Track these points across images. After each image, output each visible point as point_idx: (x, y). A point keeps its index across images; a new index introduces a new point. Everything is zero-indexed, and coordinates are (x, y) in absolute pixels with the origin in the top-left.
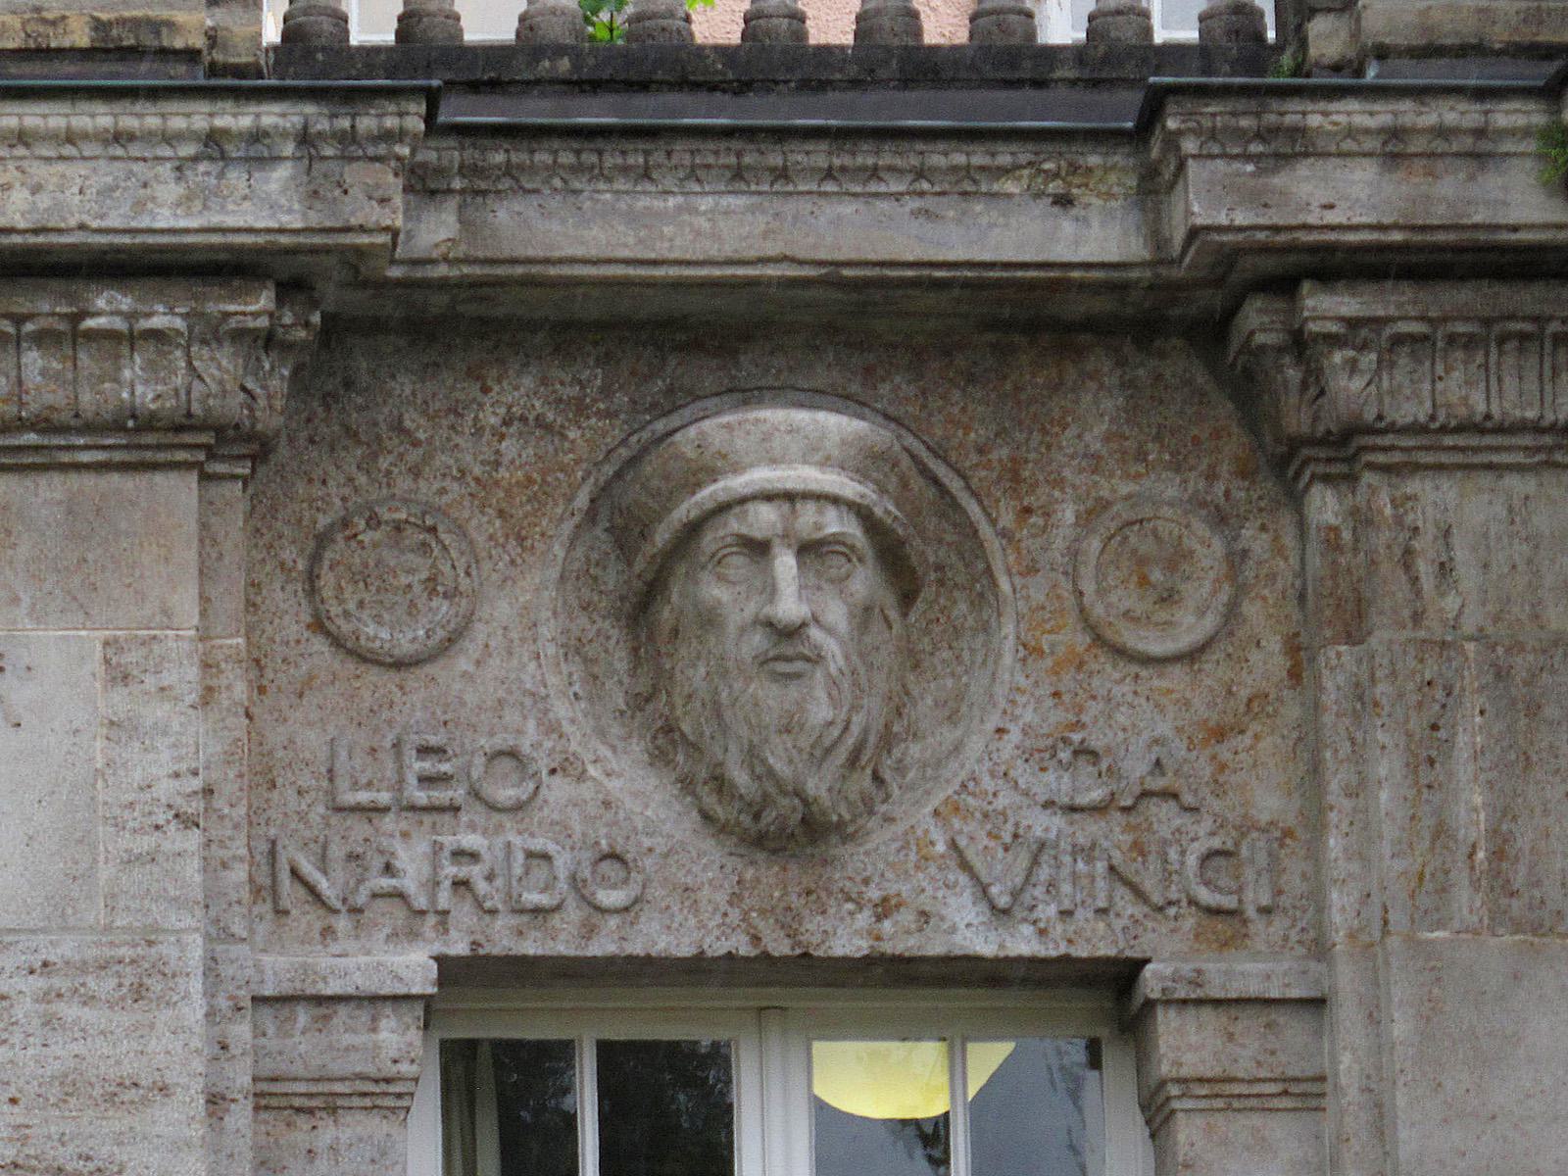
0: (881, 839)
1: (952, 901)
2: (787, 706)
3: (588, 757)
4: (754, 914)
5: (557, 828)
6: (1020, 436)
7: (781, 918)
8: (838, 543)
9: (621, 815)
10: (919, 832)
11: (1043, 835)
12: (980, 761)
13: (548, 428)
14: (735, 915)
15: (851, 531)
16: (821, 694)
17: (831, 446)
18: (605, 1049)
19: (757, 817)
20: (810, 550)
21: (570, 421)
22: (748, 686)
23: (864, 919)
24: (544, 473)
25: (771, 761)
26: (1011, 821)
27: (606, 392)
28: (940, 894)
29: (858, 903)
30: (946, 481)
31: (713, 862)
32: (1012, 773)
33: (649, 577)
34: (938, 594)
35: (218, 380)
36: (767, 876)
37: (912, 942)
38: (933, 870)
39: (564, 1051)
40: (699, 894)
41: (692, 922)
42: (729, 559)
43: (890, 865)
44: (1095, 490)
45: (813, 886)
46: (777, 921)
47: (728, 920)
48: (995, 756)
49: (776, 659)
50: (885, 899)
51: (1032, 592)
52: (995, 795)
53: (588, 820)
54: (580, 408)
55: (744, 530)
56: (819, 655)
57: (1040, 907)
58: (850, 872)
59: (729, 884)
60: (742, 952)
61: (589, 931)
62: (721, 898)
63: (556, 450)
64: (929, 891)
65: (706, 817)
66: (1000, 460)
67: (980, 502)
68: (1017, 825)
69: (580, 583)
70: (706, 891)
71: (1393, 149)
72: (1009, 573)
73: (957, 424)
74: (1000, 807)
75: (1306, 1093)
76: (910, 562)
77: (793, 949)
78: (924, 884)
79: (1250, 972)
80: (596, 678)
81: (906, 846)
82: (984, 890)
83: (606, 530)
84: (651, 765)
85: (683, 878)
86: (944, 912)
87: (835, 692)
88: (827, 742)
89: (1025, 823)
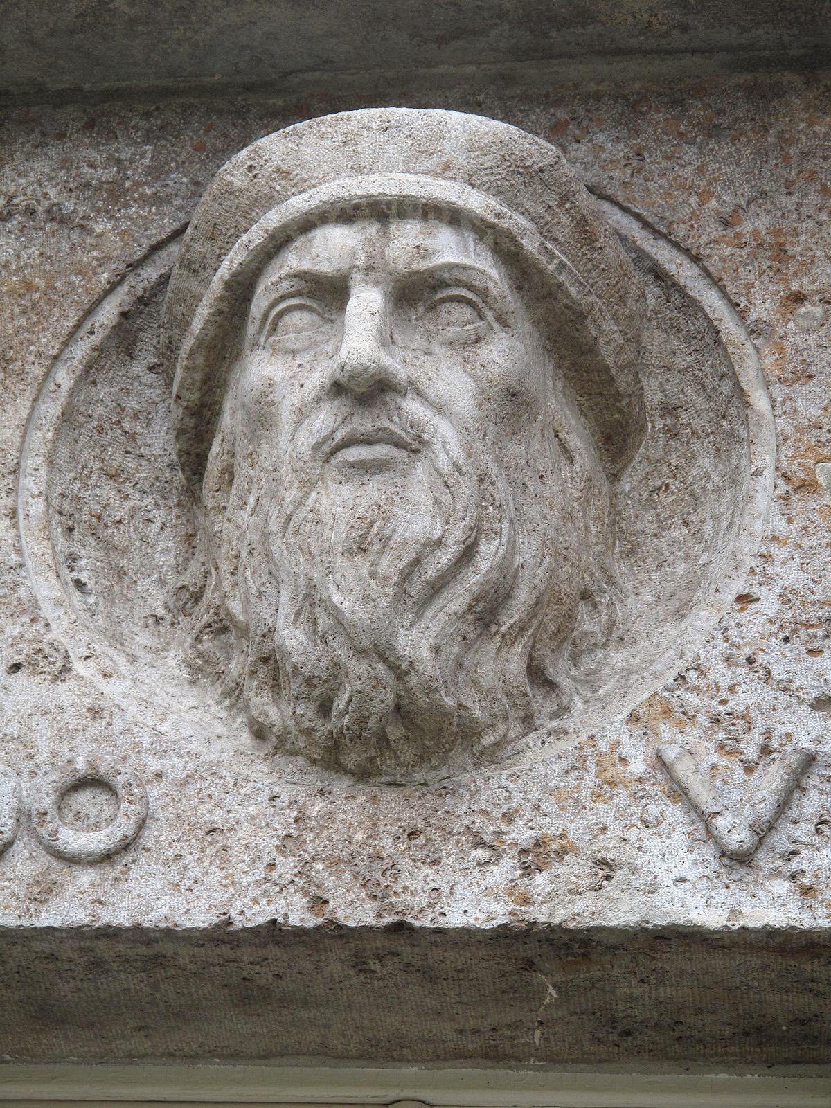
0: (542, 760)
1: (654, 844)
2: (360, 511)
3: (76, 651)
4: (320, 866)
5: (12, 746)
6: (788, 202)
7: (363, 870)
8: (459, 284)
9: (118, 726)
10: (603, 746)
11: (812, 747)
12: (710, 640)
13: (56, 216)
14: (287, 867)
15: (479, 265)
16: (423, 499)
17: (452, 148)
19: (325, 709)
21: (98, 211)
22: (307, 496)
23: (504, 871)
24: (51, 278)
25: (336, 599)
26: (759, 727)
27: (156, 172)
28: (632, 835)
29: (493, 848)
30: (671, 268)
31: (258, 791)
32: (761, 658)
33: (194, 396)
34: (667, 449)
36: (346, 810)
37: (580, 905)
38: (623, 799)
40: (233, 837)
41: (216, 876)
42: (287, 319)
43: (553, 793)
45: (420, 824)
46: (356, 875)
47: (274, 875)
48: (733, 633)
49: (346, 444)
50: (539, 843)
51: (801, 405)
52: (732, 689)
53: (62, 734)
54: (115, 194)
55: (306, 265)
56: (422, 442)
57: (805, 853)
58: (483, 802)
59: (283, 822)
60: (294, 921)
61: (44, 891)
62: (268, 843)
63: (73, 248)
64: (615, 831)
65: (259, 733)
66: (755, 232)
67: (722, 291)
68: (768, 734)
69: (106, 440)
70: (244, 832)
72: (767, 385)
73: (689, 189)
74: (741, 707)
77: (379, 915)
78: (608, 821)
80: (122, 574)
81: (579, 765)
82: (706, 820)
83: (151, 369)
84: (193, 683)
85: (209, 815)
86: (639, 862)
87: (446, 497)
88: (431, 571)
89: (781, 730)
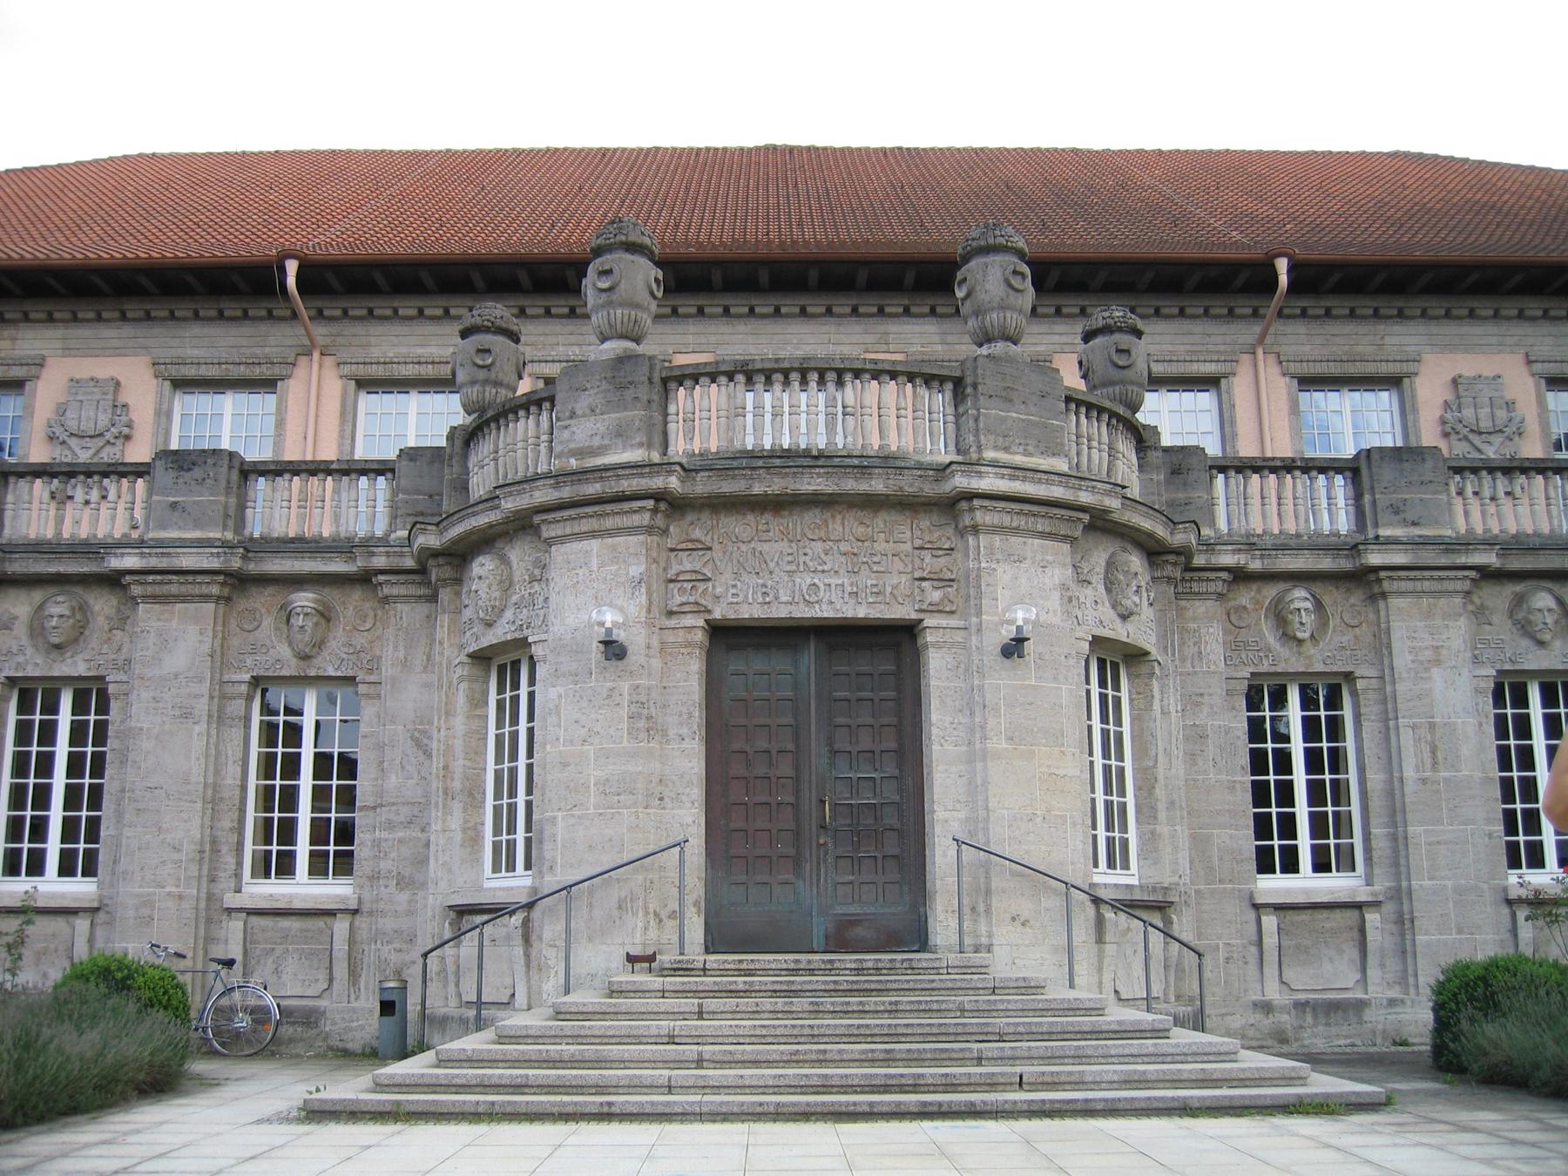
18: (1510, 684)
20: (306, 614)
35: (215, 590)
36: (301, 663)
39: (36, 690)
44: (351, 604)
71: (388, 554)
75: (378, 696)
76: (325, 615)
79: (373, 678)
